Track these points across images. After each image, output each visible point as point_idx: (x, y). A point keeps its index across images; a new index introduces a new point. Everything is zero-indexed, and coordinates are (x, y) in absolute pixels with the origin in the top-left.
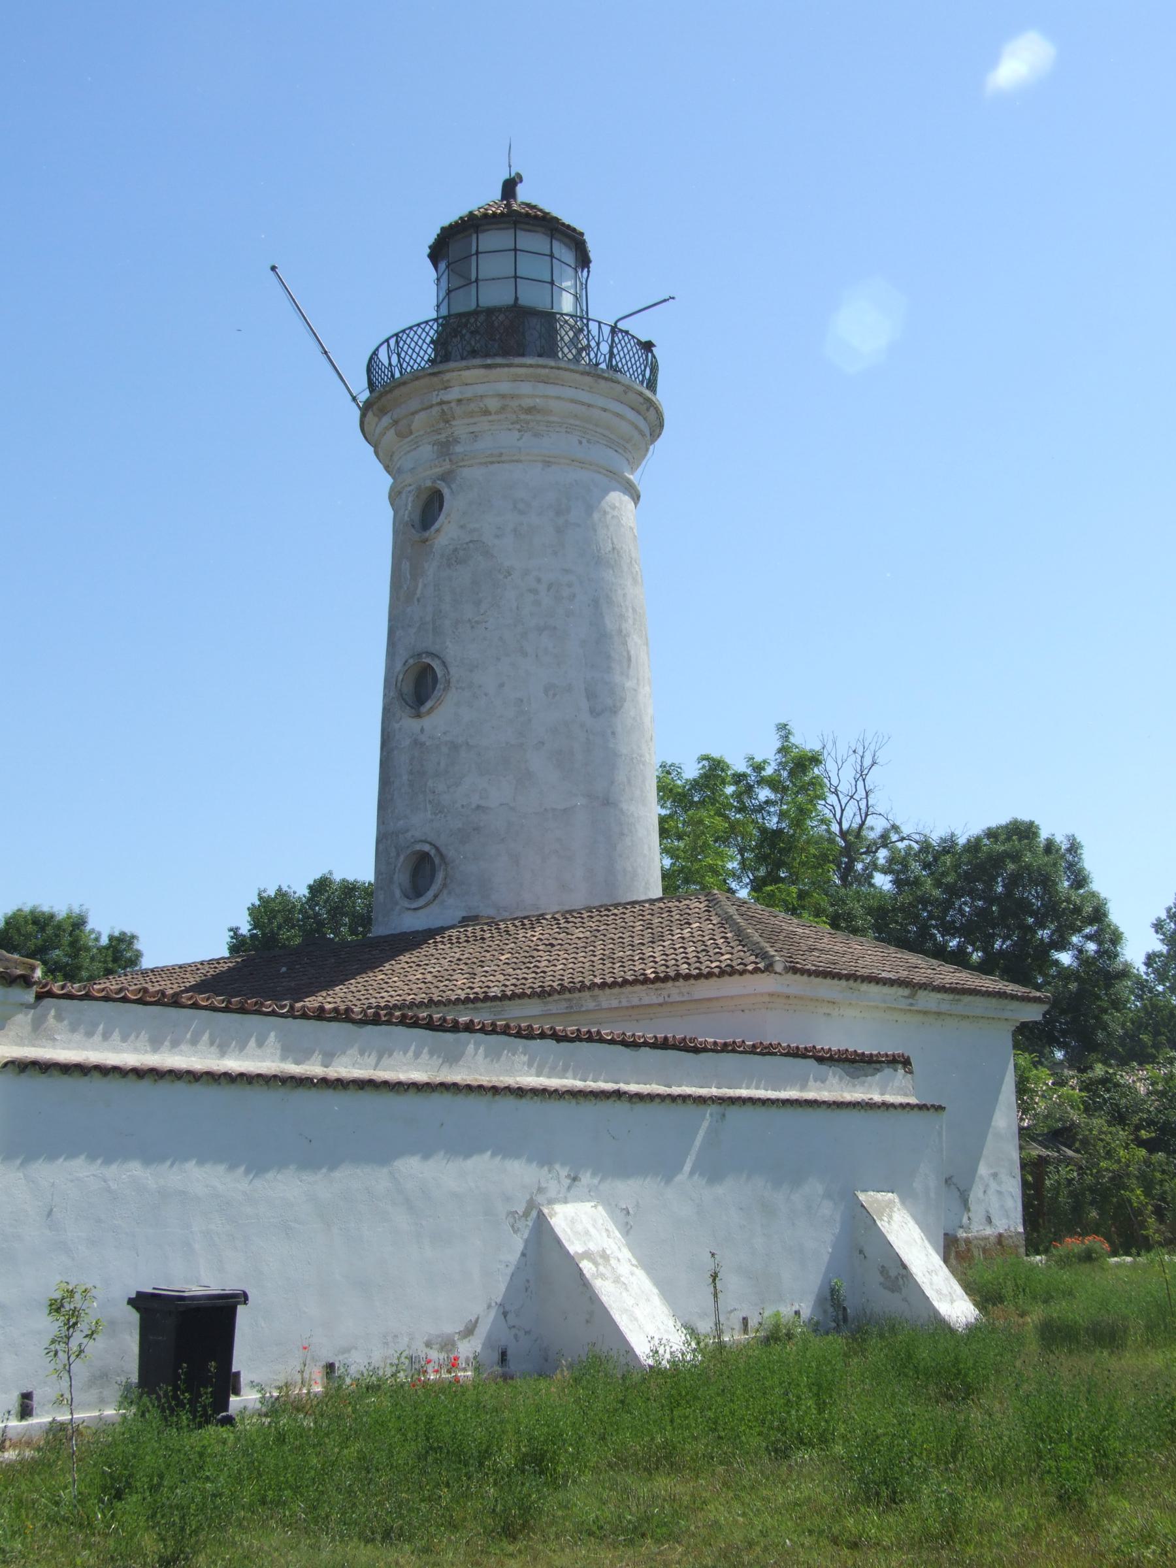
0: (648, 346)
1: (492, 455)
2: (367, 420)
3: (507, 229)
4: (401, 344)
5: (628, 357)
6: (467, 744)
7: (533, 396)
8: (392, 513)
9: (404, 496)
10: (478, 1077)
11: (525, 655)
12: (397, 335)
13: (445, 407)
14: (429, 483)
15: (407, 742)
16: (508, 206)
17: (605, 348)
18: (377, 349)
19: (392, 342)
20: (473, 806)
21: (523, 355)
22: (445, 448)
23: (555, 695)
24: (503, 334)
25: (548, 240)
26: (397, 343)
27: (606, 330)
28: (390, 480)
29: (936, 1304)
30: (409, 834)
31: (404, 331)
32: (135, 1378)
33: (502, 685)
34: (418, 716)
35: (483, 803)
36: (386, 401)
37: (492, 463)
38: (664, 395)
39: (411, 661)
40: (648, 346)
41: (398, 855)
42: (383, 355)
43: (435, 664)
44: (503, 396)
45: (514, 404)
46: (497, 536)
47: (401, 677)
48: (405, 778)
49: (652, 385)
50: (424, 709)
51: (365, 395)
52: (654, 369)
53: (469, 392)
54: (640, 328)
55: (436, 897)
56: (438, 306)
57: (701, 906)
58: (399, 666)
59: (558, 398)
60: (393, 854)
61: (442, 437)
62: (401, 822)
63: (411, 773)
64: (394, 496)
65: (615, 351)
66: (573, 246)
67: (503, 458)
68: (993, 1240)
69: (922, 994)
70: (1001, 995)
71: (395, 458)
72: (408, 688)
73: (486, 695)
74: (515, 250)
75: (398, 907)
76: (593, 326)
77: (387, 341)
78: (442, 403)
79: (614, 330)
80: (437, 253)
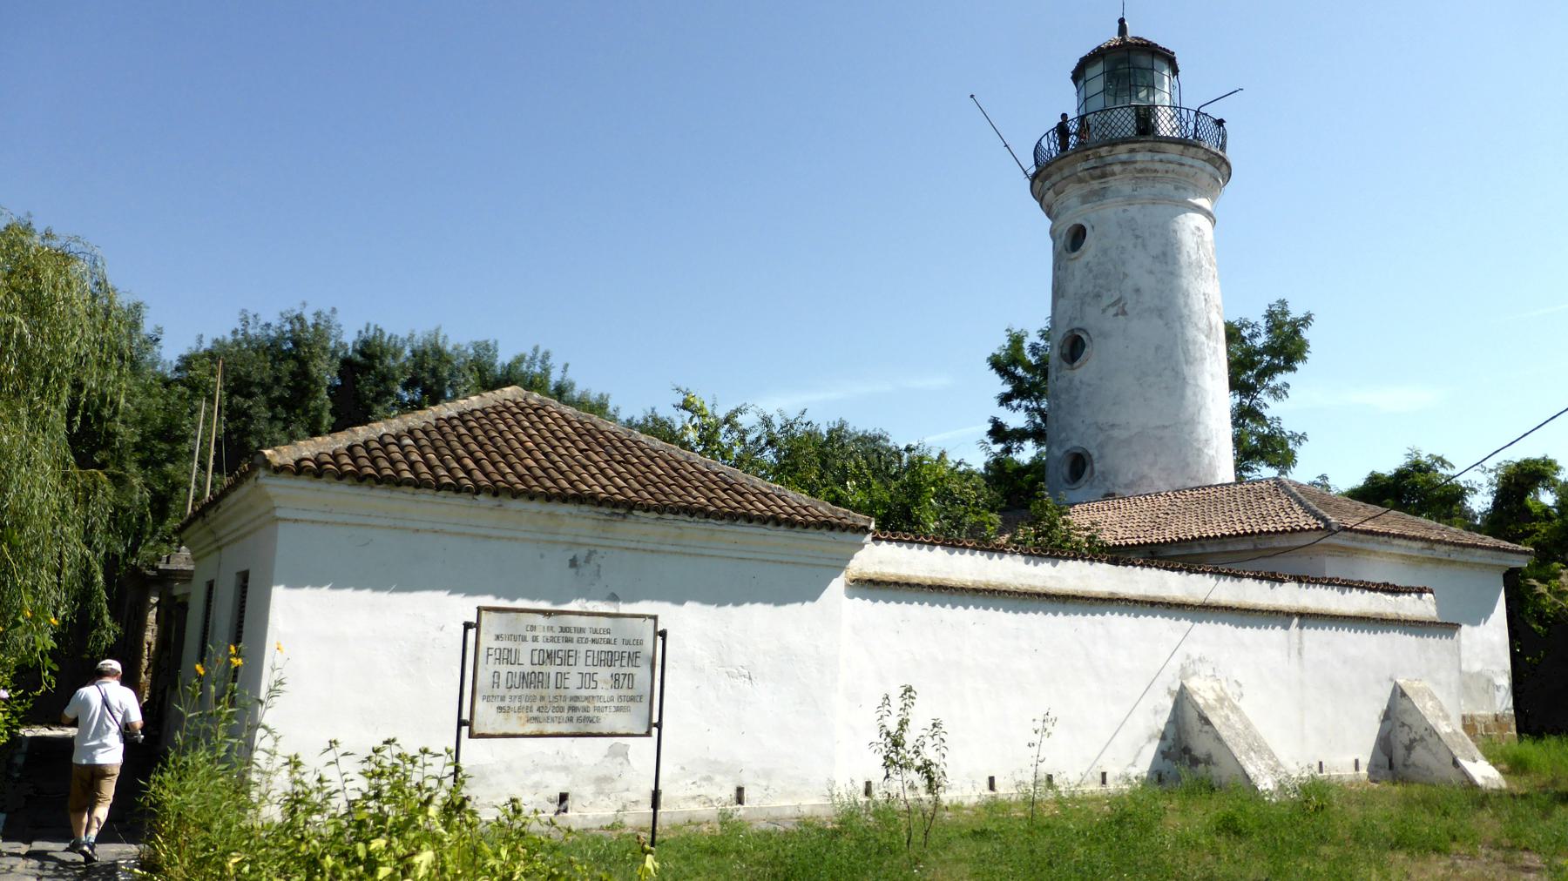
0: (1220, 123)
5: (1207, 127)
8: (1051, 243)
10: (1210, 269)
16: (1123, 39)
17: (1191, 126)
24: (1120, 132)
27: (1192, 114)
29: (1242, 759)
32: (1503, 703)
36: (1045, 178)
38: (1230, 154)
40: (1220, 123)
42: (1044, 143)
43: (1084, 337)
45: (1131, 167)
49: (1223, 147)
51: (1034, 170)
52: (1224, 137)
54: (1215, 112)
64: (1052, 233)
68: (1492, 719)
69: (1436, 546)
70: (1497, 549)
72: (1066, 350)
76: (1184, 112)
79: (1197, 113)
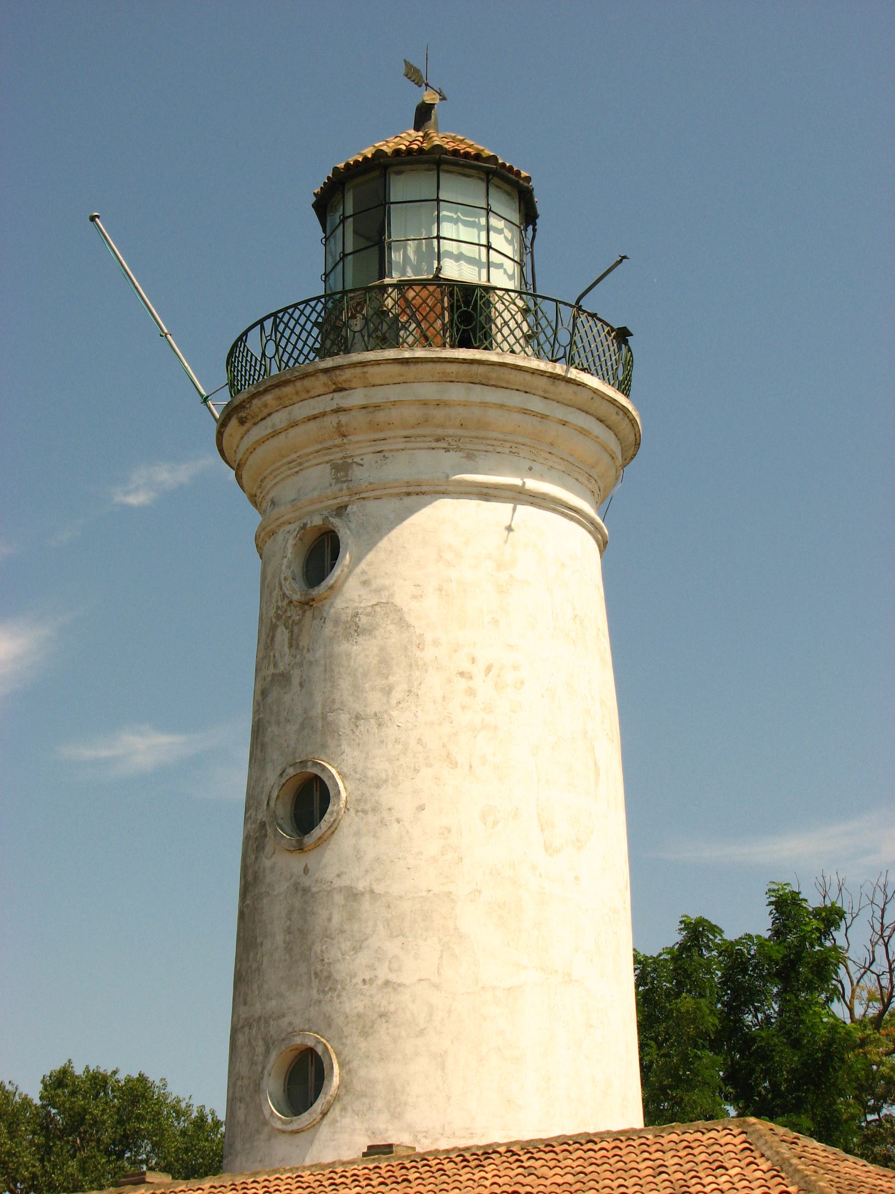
0: (622, 335)
1: (408, 484)
2: (228, 431)
3: (429, 170)
4: (281, 327)
6: (372, 891)
7: (466, 404)
9: (280, 537)
11: (454, 764)
12: (274, 315)
13: (344, 418)
14: (317, 521)
15: (283, 887)
18: (245, 333)
19: (268, 324)
20: (380, 982)
21: (347, 351)
22: (342, 469)
23: (496, 823)
25: (483, 185)
26: (275, 326)
27: (567, 313)
28: (261, 519)
30: (286, 1020)
31: (285, 310)
33: (421, 808)
34: (300, 848)
35: (392, 977)
37: (409, 494)
39: (291, 771)
40: (622, 335)
41: (268, 1051)
42: (254, 343)
44: (425, 403)
45: (439, 414)
46: (414, 597)
47: (275, 794)
48: (280, 939)
50: (309, 840)
52: (629, 364)
53: (378, 395)
55: (324, 1114)
56: (327, 275)
57: (737, 1141)
58: (272, 777)
59: (501, 406)
60: (260, 1049)
61: (337, 456)
62: (274, 1002)
63: (288, 931)
64: (263, 540)
65: (577, 338)
66: (516, 194)
67: (424, 489)
71: (268, 484)
73: (398, 821)
74: (438, 200)
75: (266, 1130)
77: (261, 322)
78: (338, 410)
80: (324, 204)
